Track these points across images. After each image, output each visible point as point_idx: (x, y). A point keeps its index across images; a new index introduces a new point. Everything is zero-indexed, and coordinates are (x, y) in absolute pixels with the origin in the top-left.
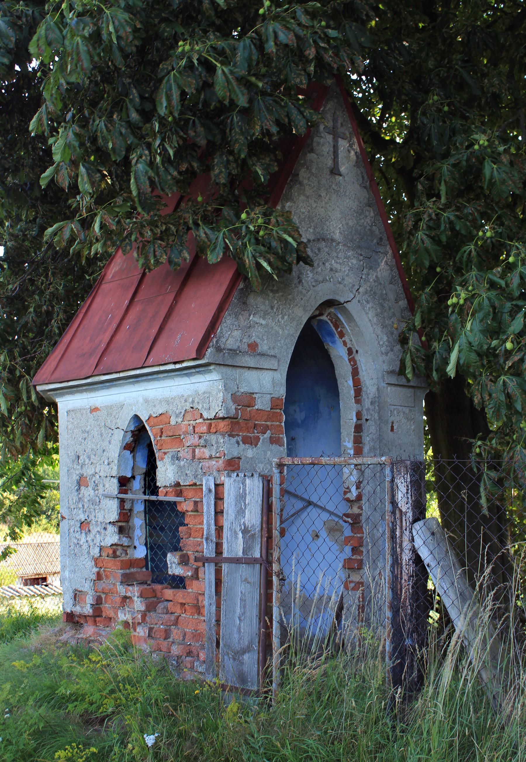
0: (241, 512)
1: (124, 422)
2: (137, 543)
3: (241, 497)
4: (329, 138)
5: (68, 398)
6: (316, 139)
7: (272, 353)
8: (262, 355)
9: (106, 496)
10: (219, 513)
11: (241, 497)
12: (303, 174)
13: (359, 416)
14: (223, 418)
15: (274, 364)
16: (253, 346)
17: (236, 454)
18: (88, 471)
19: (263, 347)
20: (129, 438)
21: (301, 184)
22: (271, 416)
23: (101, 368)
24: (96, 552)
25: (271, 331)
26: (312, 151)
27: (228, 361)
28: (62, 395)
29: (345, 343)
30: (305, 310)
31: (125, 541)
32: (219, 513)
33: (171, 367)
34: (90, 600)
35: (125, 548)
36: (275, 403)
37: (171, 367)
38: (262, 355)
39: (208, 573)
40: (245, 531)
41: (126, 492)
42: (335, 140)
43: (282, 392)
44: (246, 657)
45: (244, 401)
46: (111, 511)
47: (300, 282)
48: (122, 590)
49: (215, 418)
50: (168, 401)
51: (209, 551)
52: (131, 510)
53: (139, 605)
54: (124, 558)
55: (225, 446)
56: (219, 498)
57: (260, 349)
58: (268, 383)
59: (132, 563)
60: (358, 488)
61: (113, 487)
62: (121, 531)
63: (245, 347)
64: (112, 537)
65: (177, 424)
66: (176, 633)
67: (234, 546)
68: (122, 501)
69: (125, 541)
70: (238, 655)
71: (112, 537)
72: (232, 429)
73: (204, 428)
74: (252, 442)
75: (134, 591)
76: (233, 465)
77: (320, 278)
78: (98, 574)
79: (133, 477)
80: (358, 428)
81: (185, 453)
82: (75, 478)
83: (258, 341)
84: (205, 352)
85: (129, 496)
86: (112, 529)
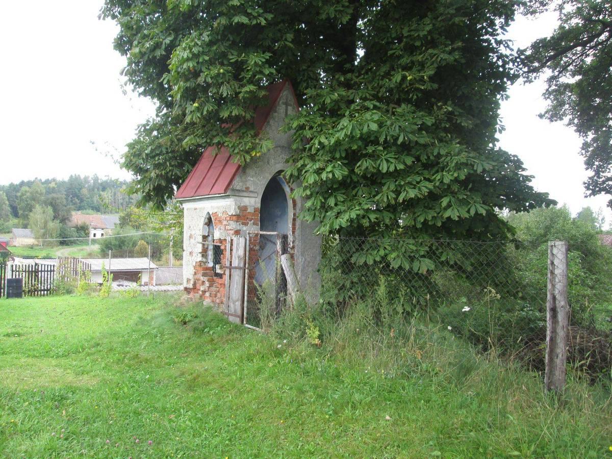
0: (237, 250)
1: (205, 214)
2: (209, 261)
3: (238, 244)
4: (284, 106)
5: (187, 204)
6: (278, 107)
7: (255, 191)
8: (251, 192)
9: (198, 243)
10: (231, 250)
11: (238, 244)
12: (272, 122)
13: (294, 215)
14: (235, 215)
15: (256, 195)
16: (247, 188)
17: (239, 228)
18: (193, 233)
19: (252, 189)
20: (207, 221)
21: (270, 125)
22: (253, 214)
23: (197, 193)
24: (194, 264)
25: (258, 182)
26: (276, 112)
27: (237, 193)
28: (185, 203)
29: (289, 186)
30: (270, 173)
31: (204, 260)
32: (231, 250)
33: (218, 195)
34: (192, 282)
35: (205, 263)
36: (256, 210)
37: (218, 195)
38: (251, 192)
39: (227, 272)
40: (239, 257)
41: (205, 241)
42: (287, 107)
43: (259, 205)
44: (237, 303)
45: (243, 209)
46: (199, 248)
47: (268, 163)
48: (202, 278)
49: (232, 215)
50: (218, 208)
51: (228, 264)
52: (207, 248)
53: (207, 284)
54: (204, 266)
55: (233, 225)
56: (232, 245)
57: (250, 190)
58: (253, 202)
59: (207, 269)
60: (293, 243)
61: (200, 239)
62: (203, 256)
63: (244, 189)
64: (199, 258)
65: (221, 217)
66: (219, 295)
67: (235, 263)
68: (203, 245)
69: (204, 260)
70: (234, 302)
71: (199, 258)
72: (238, 219)
73: (228, 219)
74: (245, 224)
75: (205, 279)
76: (237, 233)
77: (277, 161)
78: (195, 272)
79: (209, 235)
80: (294, 220)
81: (222, 227)
82: (189, 235)
83: (250, 186)
84: (229, 191)
85: (207, 243)
86: (200, 255)
